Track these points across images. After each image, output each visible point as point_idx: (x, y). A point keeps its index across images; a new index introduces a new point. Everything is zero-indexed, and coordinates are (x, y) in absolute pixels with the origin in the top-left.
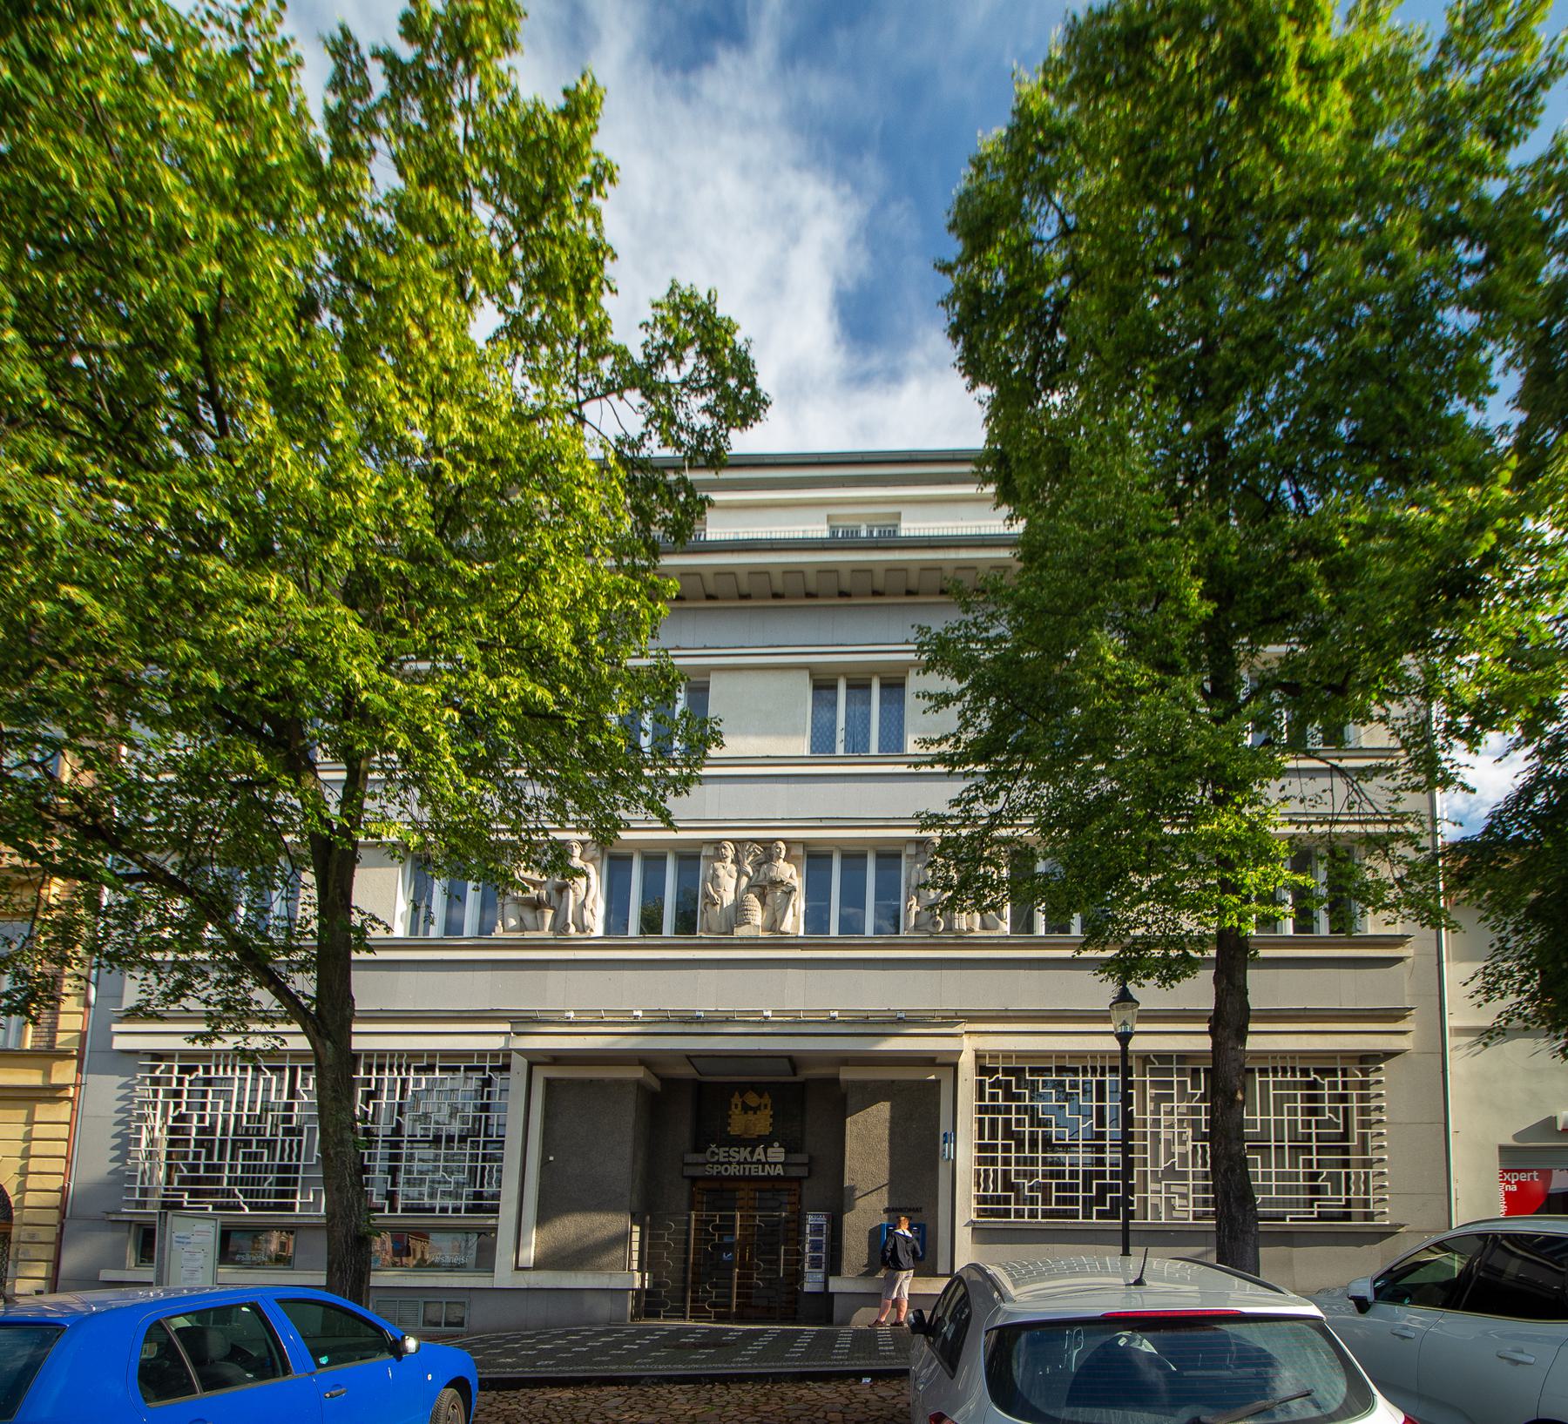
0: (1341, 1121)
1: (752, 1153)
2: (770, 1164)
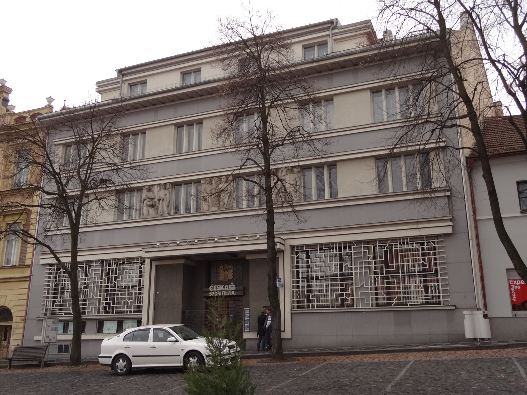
0: (427, 264)
1: (224, 287)
2: (230, 291)
